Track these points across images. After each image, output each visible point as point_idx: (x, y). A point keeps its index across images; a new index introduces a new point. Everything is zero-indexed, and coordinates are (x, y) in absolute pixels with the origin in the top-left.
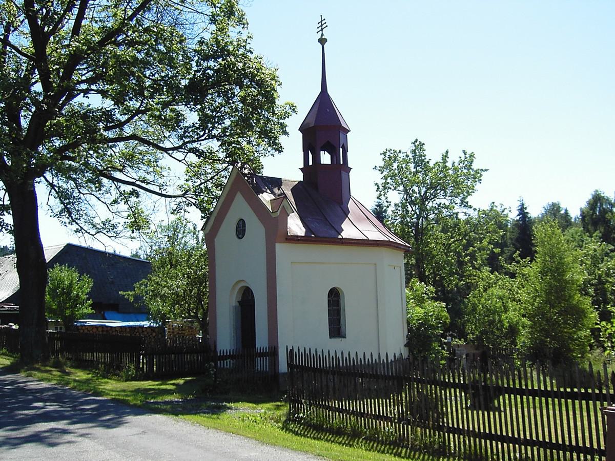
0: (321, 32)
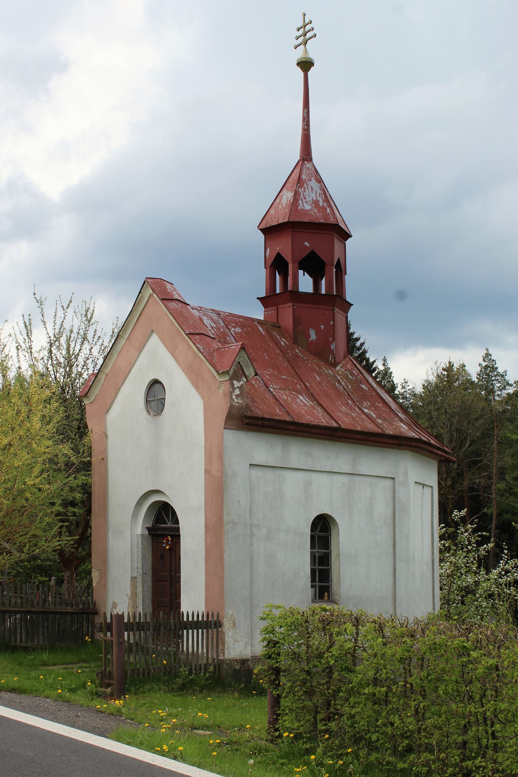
0: (302, 46)
